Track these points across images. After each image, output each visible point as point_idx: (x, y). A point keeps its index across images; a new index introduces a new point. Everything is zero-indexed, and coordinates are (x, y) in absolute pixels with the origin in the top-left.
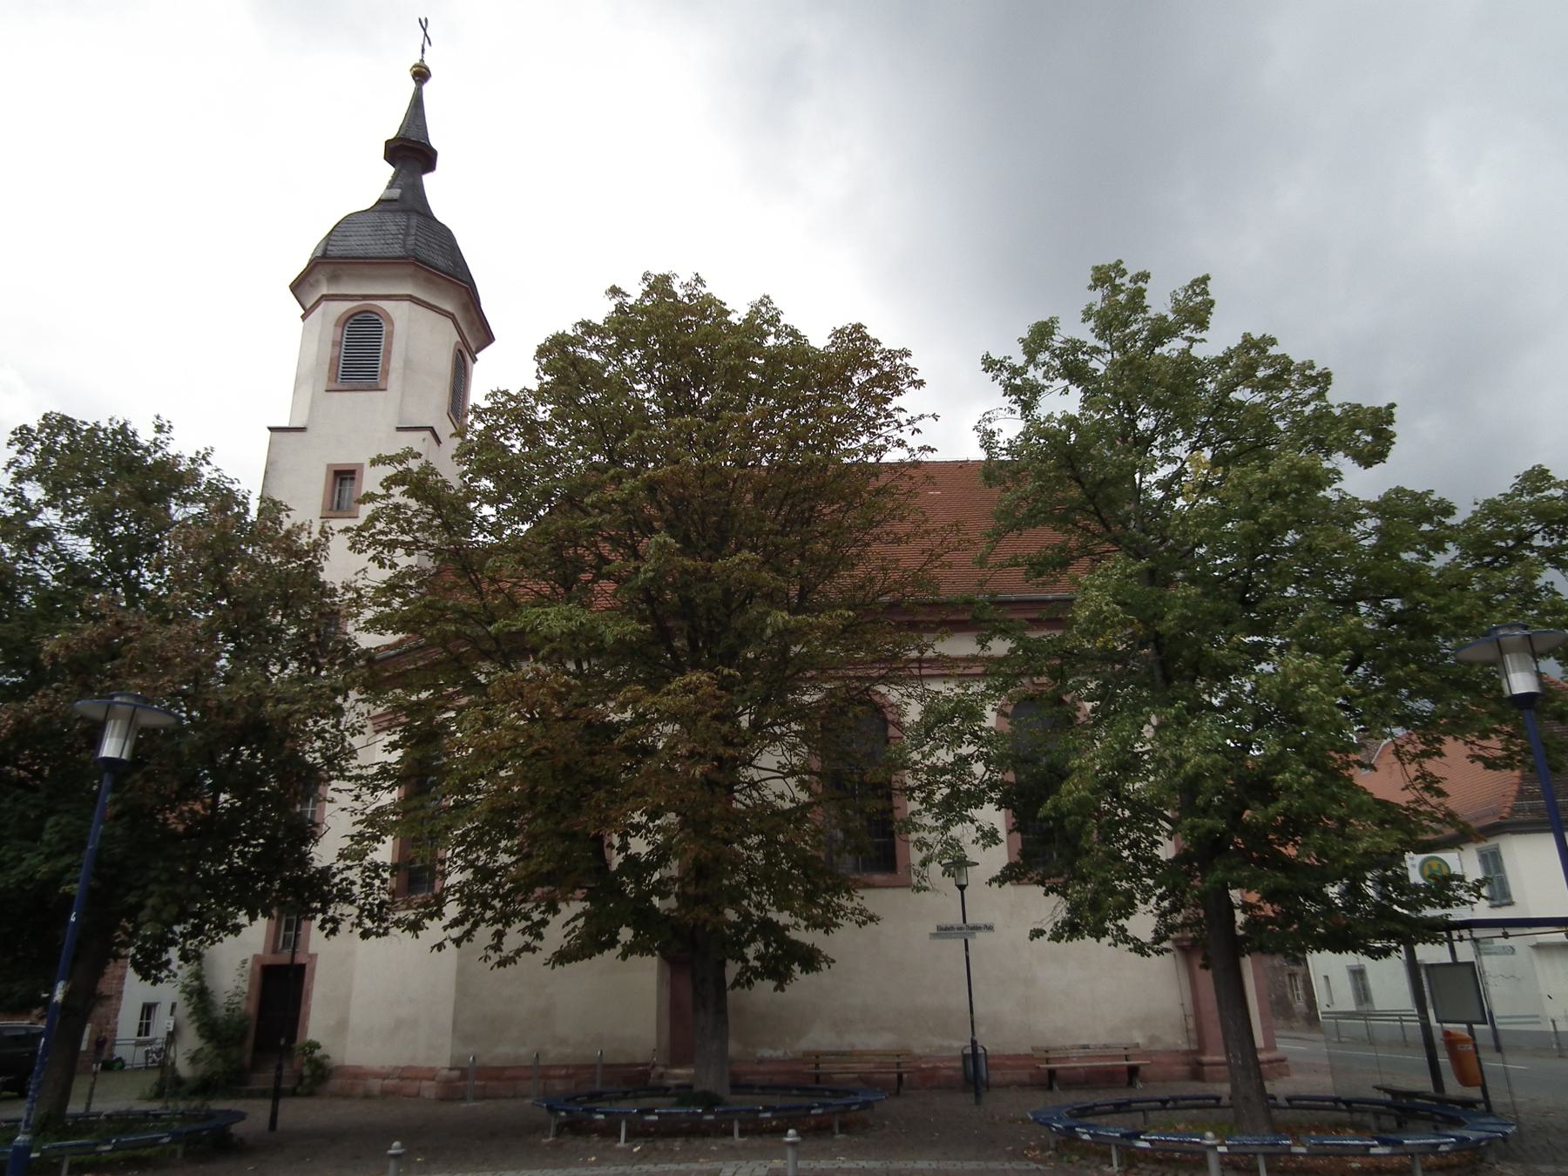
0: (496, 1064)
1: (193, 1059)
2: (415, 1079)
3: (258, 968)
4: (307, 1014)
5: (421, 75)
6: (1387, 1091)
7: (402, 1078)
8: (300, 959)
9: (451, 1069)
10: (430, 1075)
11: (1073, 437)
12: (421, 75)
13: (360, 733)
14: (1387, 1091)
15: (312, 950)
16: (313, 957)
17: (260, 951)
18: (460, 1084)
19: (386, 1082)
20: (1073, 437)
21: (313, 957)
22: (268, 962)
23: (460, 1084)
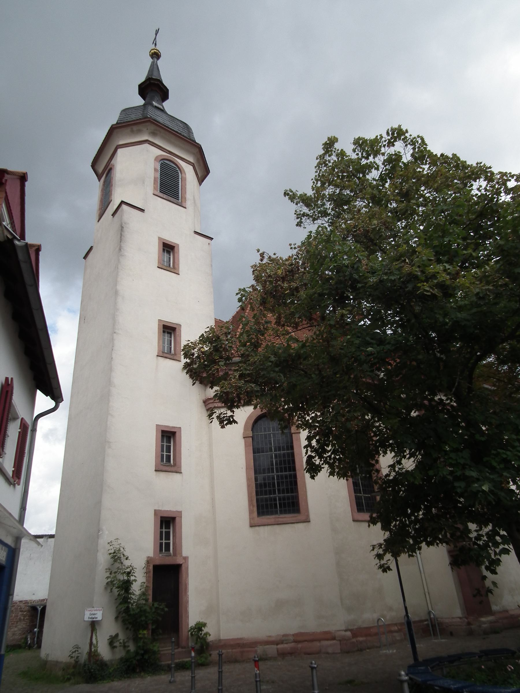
0: (365, 625)
1: (112, 642)
2: (312, 641)
3: (151, 568)
4: (187, 602)
5: (156, 55)
6: (239, 307)
7: (295, 641)
8: (179, 561)
9: (346, 631)
10: (329, 636)
11: (437, 202)
12: (156, 55)
13: (230, 423)
14: (239, 307)
15: (185, 553)
16: (186, 559)
17: (151, 554)
18: (354, 640)
19: (280, 646)
20: (437, 202)
21: (186, 559)
22: (158, 562)
23: (354, 640)
